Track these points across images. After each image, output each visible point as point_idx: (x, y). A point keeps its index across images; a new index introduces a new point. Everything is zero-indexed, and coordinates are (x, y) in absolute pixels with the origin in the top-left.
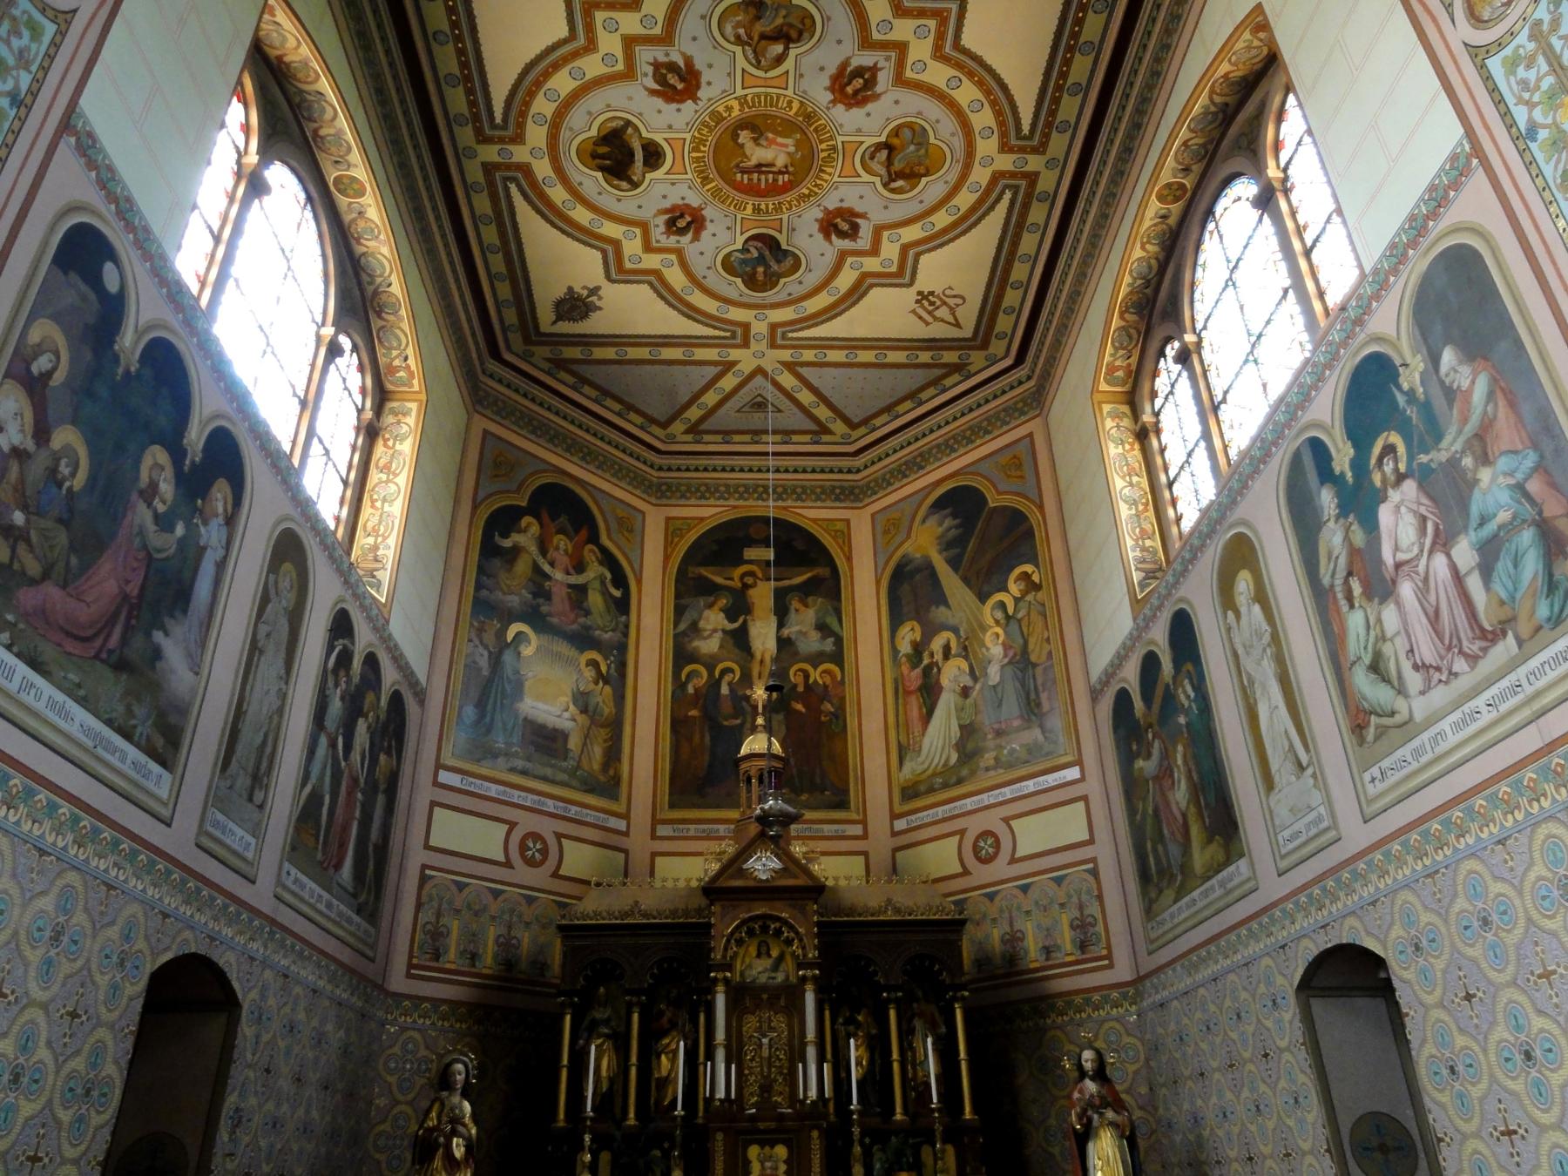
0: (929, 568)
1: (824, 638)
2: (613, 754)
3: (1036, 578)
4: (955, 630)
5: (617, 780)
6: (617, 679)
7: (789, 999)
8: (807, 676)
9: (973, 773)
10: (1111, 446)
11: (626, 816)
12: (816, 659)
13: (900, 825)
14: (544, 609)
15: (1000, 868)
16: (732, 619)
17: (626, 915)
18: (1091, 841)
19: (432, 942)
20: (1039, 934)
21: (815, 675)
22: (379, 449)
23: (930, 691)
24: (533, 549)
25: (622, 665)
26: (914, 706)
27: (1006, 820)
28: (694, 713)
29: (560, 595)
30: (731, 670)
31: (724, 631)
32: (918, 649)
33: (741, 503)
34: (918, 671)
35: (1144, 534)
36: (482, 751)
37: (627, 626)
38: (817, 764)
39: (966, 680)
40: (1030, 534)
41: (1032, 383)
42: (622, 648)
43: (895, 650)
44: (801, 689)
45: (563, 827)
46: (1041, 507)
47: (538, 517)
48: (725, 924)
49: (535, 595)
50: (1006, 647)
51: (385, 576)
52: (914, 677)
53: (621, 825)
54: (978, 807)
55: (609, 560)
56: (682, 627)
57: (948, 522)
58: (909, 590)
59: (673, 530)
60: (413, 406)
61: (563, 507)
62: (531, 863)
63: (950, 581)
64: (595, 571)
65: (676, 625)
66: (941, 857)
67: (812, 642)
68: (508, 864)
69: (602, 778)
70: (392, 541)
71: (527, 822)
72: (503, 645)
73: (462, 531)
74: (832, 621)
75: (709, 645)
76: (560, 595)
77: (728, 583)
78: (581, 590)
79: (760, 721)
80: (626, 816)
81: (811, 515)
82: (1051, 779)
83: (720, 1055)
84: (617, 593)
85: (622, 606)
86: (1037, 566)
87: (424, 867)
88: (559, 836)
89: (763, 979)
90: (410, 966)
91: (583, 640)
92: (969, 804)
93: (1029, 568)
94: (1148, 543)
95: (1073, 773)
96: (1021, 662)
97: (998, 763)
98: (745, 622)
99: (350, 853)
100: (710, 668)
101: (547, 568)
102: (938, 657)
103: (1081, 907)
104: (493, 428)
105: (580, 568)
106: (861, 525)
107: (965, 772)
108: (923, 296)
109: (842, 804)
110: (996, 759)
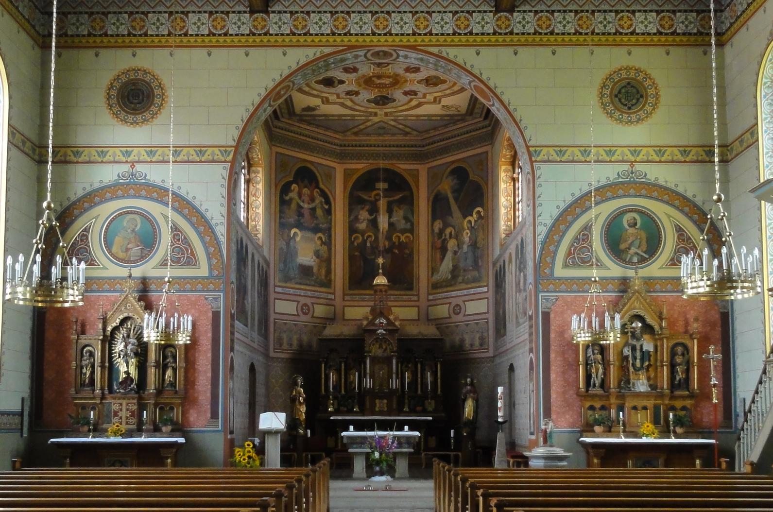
0: (447, 199)
1: (406, 223)
2: (329, 272)
3: (482, 214)
4: (454, 227)
5: (330, 281)
6: (328, 243)
7: (388, 361)
8: (399, 238)
9: (455, 284)
10: (502, 184)
11: (334, 293)
12: (403, 231)
13: (431, 297)
14: (302, 221)
15: (460, 317)
16: (371, 214)
17: (339, 336)
18: (488, 313)
19: (279, 342)
20: (470, 339)
21: (403, 238)
22: (251, 185)
23: (444, 250)
24: (297, 197)
25: (330, 236)
26: (438, 255)
27: (464, 302)
28: (357, 253)
29: (306, 213)
30: (369, 236)
31: (368, 220)
32: (441, 231)
33: (375, 162)
34: (440, 240)
35: (508, 220)
36: (287, 279)
37: (331, 219)
38: (402, 277)
39: (456, 248)
40: (482, 195)
41: (490, 128)
42: (330, 229)
43: (433, 230)
44: (397, 243)
45: (314, 300)
46: (487, 185)
47: (297, 184)
48: (369, 340)
49: (298, 216)
50: (470, 239)
51: (260, 236)
52: (439, 243)
53: (332, 297)
54: (456, 295)
55: (324, 194)
56: (352, 217)
57: (455, 181)
58: (439, 207)
59: (347, 174)
60: (260, 169)
61: (306, 176)
62: (305, 314)
63: (454, 207)
64: (319, 199)
65: (349, 216)
66: (442, 311)
67: (402, 224)
68: (298, 315)
69: (325, 281)
70: (261, 223)
71: (303, 300)
72: (290, 239)
73: (273, 198)
74: (410, 216)
75: (362, 226)
76: (306, 213)
77: (368, 198)
78: (313, 210)
79: (381, 271)
80: (334, 293)
81: (403, 167)
82: (479, 290)
83: (368, 377)
84: (327, 207)
85: (329, 212)
86: (483, 207)
87: (275, 319)
88: (313, 304)
89: (380, 355)
90: (274, 349)
91: (316, 230)
92: (453, 294)
93: (480, 209)
94: (509, 223)
95: (485, 289)
96: (474, 245)
97: (463, 282)
98: (376, 217)
99: (343, 388)
100: (363, 236)
101: (302, 204)
102: (448, 237)
103: (482, 333)
104: (279, 150)
105: (312, 199)
106: (423, 170)
107: (453, 282)
108: (443, 106)
109: (411, 289)
110: (463, 279)
